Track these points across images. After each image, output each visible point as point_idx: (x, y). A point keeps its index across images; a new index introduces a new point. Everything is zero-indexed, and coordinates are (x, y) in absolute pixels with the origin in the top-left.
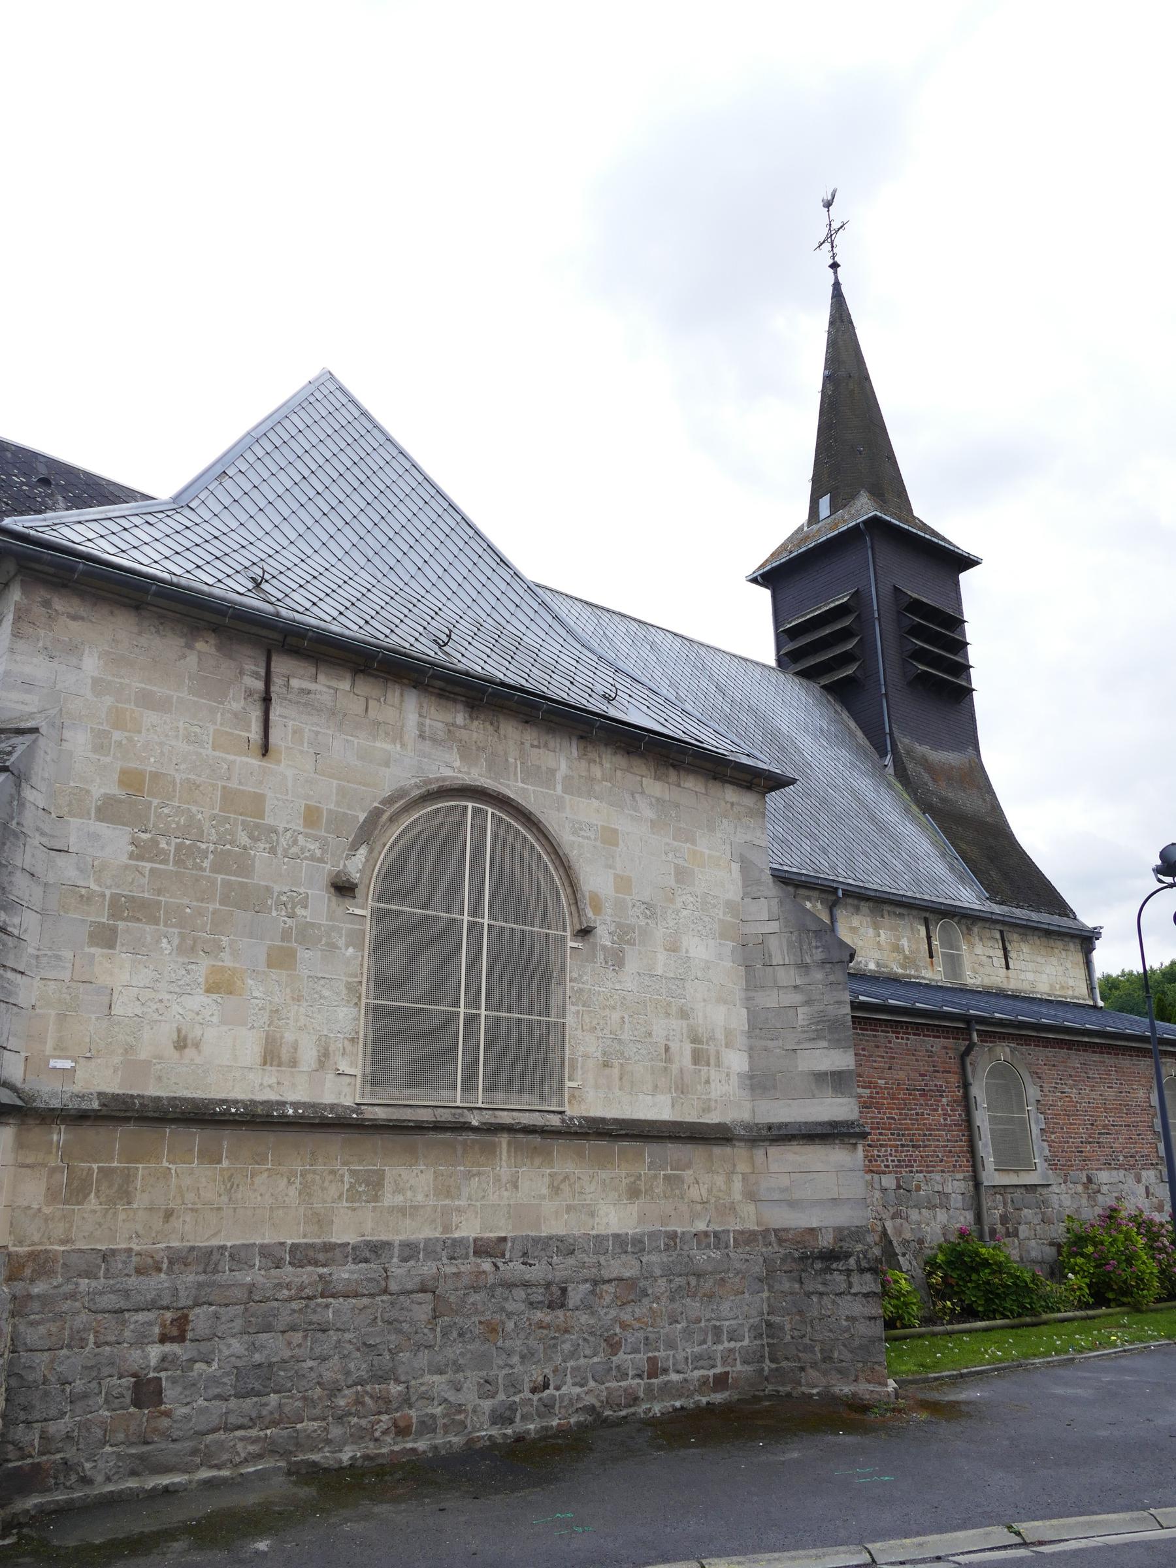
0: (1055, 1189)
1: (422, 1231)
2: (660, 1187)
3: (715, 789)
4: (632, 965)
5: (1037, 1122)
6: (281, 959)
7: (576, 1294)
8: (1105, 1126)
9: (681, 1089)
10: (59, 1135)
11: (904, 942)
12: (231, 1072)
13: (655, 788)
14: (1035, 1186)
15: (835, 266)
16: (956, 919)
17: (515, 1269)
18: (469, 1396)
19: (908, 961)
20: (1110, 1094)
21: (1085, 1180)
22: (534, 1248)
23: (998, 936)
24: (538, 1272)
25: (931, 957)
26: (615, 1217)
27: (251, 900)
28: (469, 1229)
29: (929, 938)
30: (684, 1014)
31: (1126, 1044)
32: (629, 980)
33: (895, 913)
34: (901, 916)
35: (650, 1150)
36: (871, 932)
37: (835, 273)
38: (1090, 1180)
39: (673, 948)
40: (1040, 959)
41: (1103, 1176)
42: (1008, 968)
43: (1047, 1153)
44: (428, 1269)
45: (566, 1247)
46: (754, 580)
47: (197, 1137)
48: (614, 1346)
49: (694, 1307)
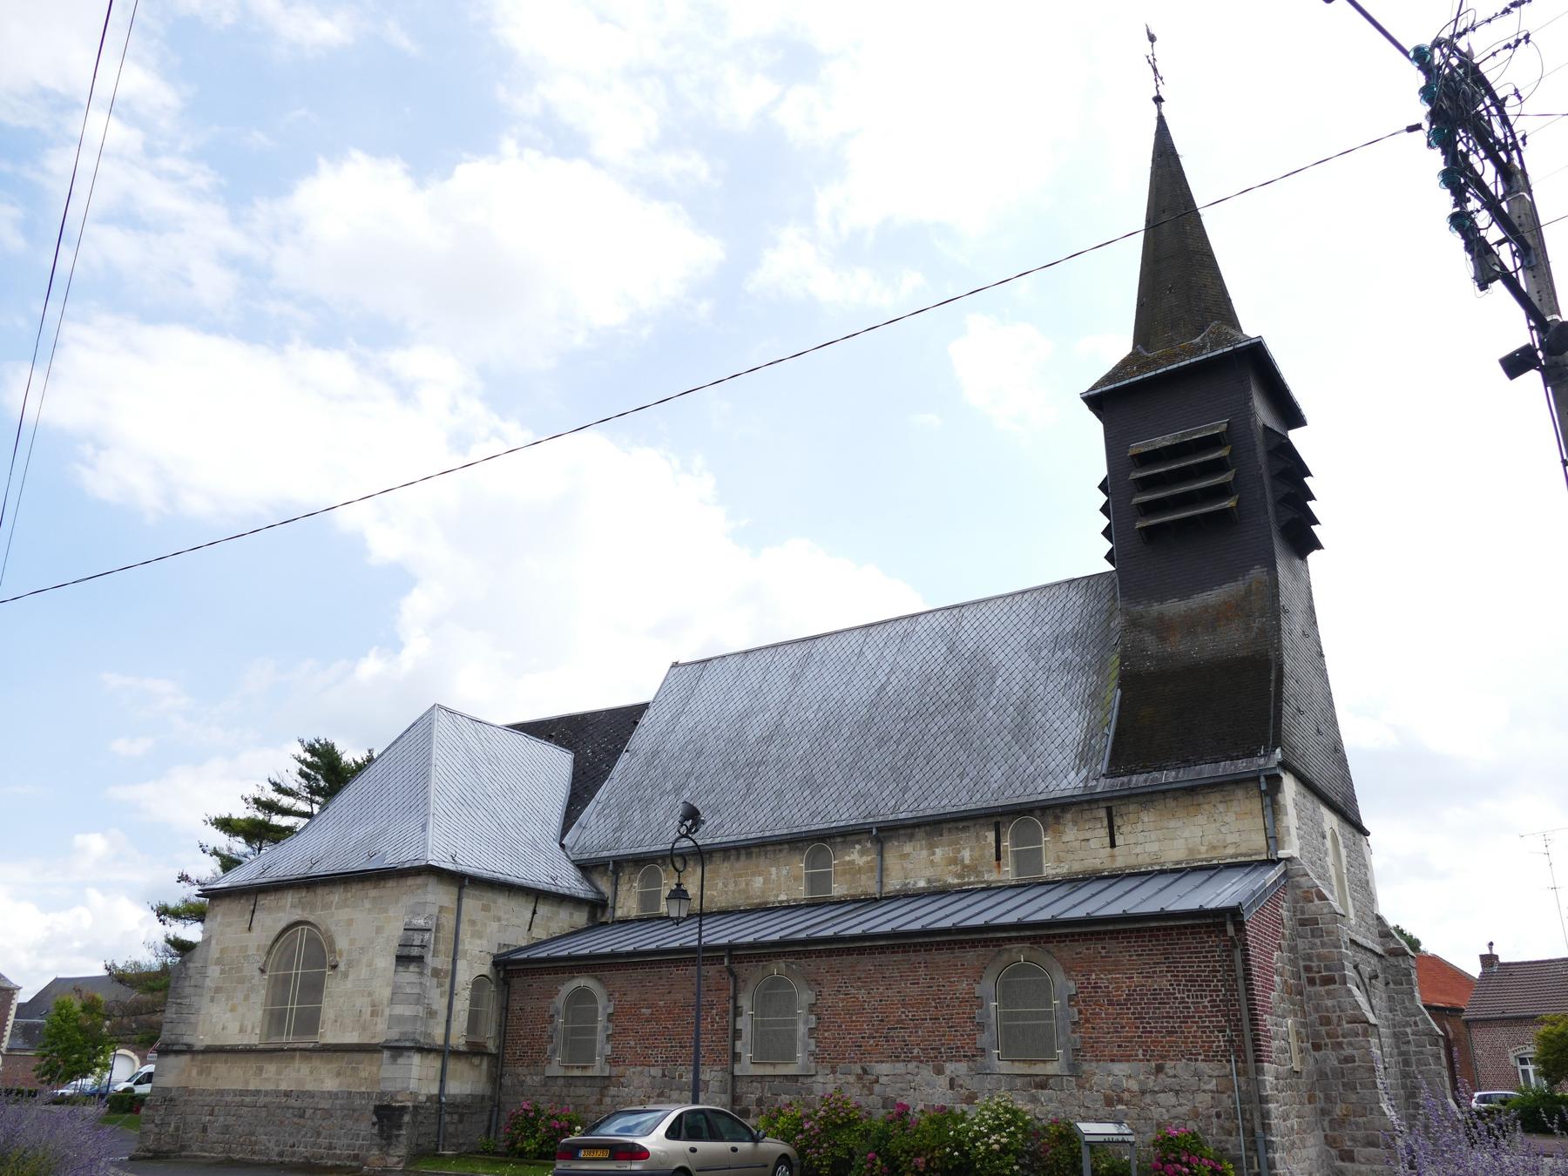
0: (820, 1079)
1: (270, 1087)
2: (349, 1072)
3: (402, 882)
4: (351, 977)
5: (806, 1022)
6: (247, 998)
7: (309, 1113)
8: (900, 1021)
9: (364, 1028)
10: (200, 1057)
11: (966, 855)
12: (233, 1038)
13: (373, 893)
14: (795, 1078)
15: (1158, 100)
16: (1038, 813)
17: (292, 1102)
18: (271, 1145)
19: (972, 869)
20: (913, 990)
21: (860, 1071)
22: (303, 1094)
23: (1103, 813)
24: (297, 1104)
25: (998, 858)
26: (330, 1084)
27: (241, 981)
28: (283, 1087)
30: (370, 994)
32: (349, 984)
34: (965, 829)
35: (347, 1056)
36: (925, 853)
37: (1159, 108)
38: (865, 1071)
39: (370, 965)
40: (1172, 824)
41: (884, 1069)
42: (1113, 845)
43: (1374, 1041)
44: (268, 1099)
45: (311, 1095)
47: (224, 1056)
48: (319, 1134)
49: (349, 1123)
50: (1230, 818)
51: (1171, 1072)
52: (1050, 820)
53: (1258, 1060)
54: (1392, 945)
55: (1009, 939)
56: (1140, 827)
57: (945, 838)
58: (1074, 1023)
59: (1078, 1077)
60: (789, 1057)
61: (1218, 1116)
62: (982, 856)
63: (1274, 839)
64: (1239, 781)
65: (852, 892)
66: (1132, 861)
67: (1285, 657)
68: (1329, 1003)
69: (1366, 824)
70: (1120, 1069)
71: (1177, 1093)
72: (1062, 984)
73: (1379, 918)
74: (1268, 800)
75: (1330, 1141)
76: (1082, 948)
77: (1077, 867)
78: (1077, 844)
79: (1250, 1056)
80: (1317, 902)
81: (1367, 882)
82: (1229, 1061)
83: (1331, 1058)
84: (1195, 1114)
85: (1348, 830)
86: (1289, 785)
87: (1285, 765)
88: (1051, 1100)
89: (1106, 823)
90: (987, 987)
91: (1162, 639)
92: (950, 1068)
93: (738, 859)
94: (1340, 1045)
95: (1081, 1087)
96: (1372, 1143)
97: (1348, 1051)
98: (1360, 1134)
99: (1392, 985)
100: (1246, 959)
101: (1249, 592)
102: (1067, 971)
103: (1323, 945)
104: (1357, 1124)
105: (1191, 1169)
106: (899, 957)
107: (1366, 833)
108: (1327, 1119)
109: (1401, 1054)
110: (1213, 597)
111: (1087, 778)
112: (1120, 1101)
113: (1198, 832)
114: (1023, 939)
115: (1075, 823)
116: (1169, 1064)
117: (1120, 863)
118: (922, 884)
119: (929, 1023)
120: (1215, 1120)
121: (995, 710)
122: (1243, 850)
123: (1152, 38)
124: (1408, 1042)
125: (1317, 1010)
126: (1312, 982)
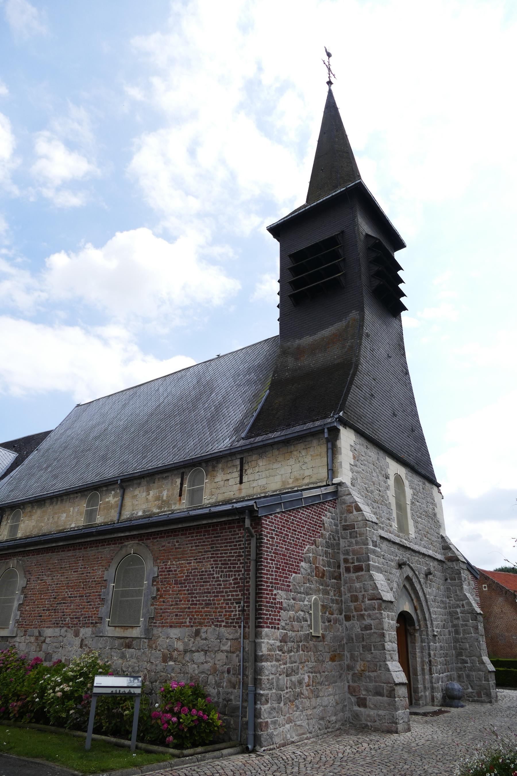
5: (18, 600)
8: (64, 599)
15: (330, 83)
16: (204, 465)
21: (37, 634)
23: (238, 462)
25: (180, 495)
29: (182, 484)
31: (83, 540)
33: (163, 478)
37: (330, 87)
40: (275, 466)
41: (49, 632)
42: (241, 482)
43: (18, 617)
46: (402, 269)
50: (308, 459)
51: (204, 636)
52: (210, 468)
53: (258, 626)
54: (450, 555)
55: (127, 538)
56: (257, 469)
57: (156, 485)
58: (154, 598)
59: (150, 639)
60: (460, 635)
61: (229, 672)
62: (173, 494)
63: (332, 471)
64: (315, 434)
65: (106, 520)
66: (250, 492)
67: (362, 360)
68: (358, 585)
69: (439, 481)
70: (175, 633)
71: (206, 652)
72: (150, 568)
73: (442, 537)
74: (330, 445)
75: (352, 691)
76: (167, 543)
77: (221, 498)
78: (222, 483)
79: (252, 622)
80: (355, 513)
81: (435, 515)
82: (240, 627)
83: (356, 626)
84: (214, 670)
85: (417, 480)
86: (347, 438)
87: (346, 424)
88: (132, 657)
89: (239, 468)
90: (110, 573)
91: (297, 359)
92: (83, 631)
93: (57, 504)
94: (362, 616)
95: (150, 647)
96: (379, 693)
97: (368, 621)
98: (371, 685)
99: (449, 581)
100: (259, 547)
101: (347, 326)
102: (155, 560)
103: (357, 543)
104: (369, 677)
105: (179, 718)
106: (70, 553)
107: (438, 486)
108: (351, 673)
109: (454, 626)
110: (327, 332)
111: (233, 441)
112: (171, 658)
113: (288, 469)
114: (133, 537)
115: (223, 469)
116: (204, 629)
117: (243, 494)
118: (140, 514)
119: (78, 600)
120: (226, 675)
121: (205, 410)
122: (313, 480)
123: (329, 55)
124: (458, 618)
125: (349, 591)
126: (348, 570)
